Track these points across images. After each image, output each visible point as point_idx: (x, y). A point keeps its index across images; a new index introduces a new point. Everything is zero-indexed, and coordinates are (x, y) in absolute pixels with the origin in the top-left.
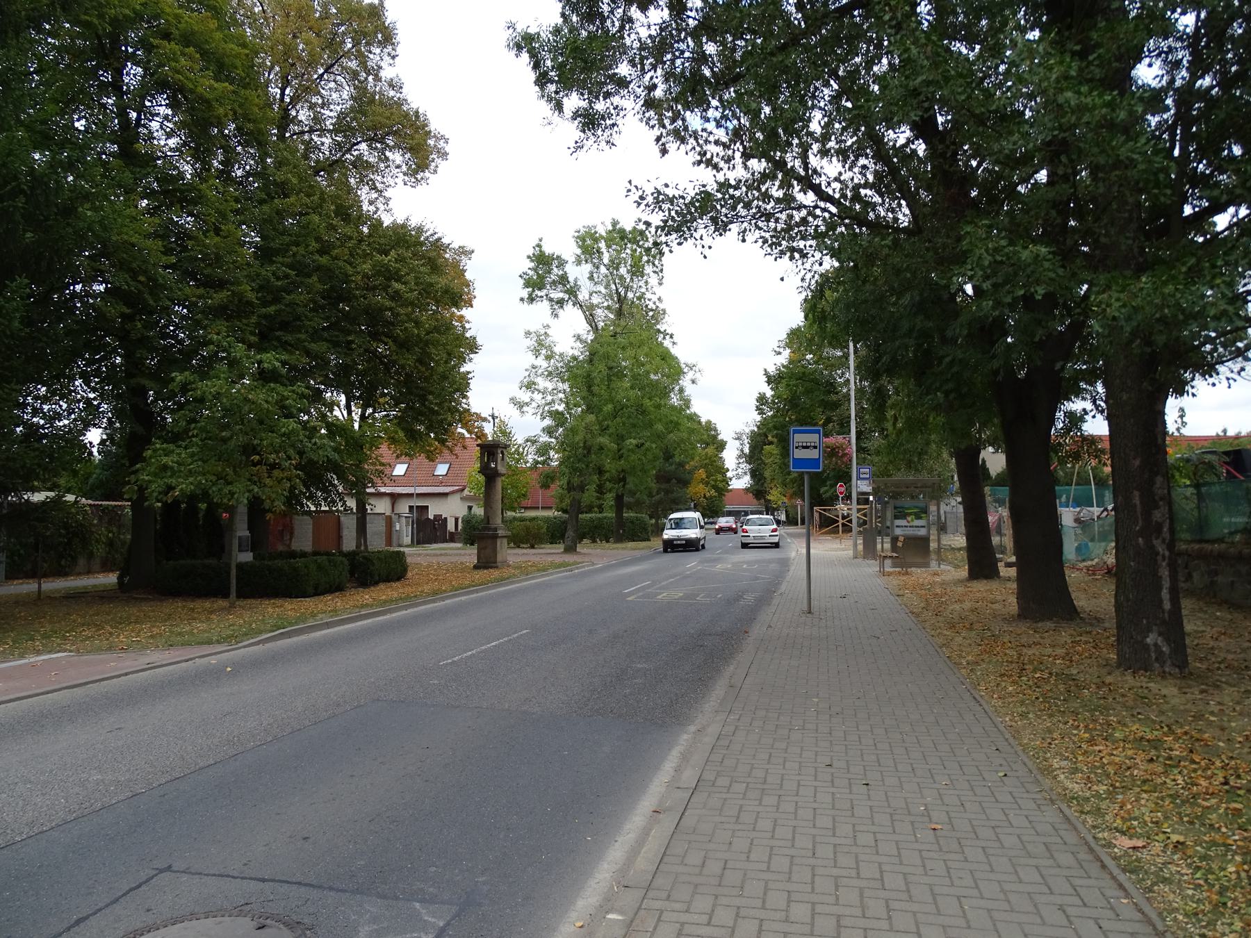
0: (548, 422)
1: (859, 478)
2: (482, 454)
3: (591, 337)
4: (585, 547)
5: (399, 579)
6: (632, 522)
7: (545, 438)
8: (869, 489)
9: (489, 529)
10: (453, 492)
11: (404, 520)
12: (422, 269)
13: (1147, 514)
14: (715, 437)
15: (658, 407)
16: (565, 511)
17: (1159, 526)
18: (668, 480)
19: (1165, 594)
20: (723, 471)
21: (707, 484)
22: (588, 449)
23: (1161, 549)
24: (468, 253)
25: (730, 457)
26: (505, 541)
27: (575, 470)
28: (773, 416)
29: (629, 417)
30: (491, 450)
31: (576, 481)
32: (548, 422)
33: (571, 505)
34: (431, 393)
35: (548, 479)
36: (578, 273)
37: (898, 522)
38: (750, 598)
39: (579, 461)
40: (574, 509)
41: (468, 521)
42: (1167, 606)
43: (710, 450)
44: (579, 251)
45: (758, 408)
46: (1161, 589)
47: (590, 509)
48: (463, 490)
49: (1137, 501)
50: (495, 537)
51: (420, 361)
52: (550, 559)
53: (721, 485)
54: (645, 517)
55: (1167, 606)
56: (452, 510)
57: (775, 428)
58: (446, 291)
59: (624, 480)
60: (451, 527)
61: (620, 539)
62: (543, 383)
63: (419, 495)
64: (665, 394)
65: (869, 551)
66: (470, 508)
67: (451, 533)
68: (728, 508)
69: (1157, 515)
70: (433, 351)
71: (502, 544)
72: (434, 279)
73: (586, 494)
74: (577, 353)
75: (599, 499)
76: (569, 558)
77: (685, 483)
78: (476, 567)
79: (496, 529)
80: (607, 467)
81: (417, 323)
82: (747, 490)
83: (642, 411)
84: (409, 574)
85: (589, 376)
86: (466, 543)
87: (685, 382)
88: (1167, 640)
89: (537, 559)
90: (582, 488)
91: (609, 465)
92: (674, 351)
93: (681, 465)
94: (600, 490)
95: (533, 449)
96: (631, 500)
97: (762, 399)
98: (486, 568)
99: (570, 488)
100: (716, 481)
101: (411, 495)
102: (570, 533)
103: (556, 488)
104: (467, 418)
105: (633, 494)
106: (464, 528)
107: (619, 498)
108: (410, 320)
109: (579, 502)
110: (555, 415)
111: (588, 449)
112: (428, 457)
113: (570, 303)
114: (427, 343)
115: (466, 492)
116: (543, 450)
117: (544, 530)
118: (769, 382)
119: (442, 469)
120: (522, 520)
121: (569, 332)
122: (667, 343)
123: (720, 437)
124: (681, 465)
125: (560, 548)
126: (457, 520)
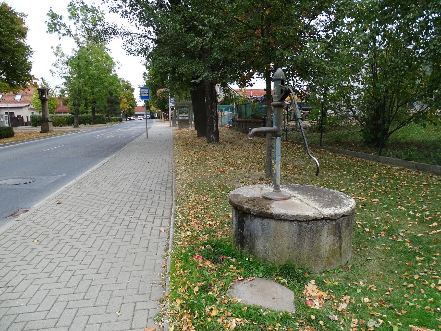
0: (64, 80)
1: (171, 102)
2: (39, 92)
3: (78, 49)
4: (82, 126)
5: (11, 137)
6: (99, 117)
7: (64, 87)
8: (174, 105)
9: (45, 119)
10: (25, 107)
11: (4, 117)
12: (9, 23)
13: (211, 110)
14: (130, 87)
15: (106, 77)
16: (73, 114)
17: (214, 112)
18: (112, 103)
19: (215, 127)
20: (134, 99)
21: (128, 104)
22: (80, 91)
23: (214, 117)
24: (25, 16)
25: (137, 94)
26: (52, 123)
27: (76, 99)
28: (149, 80)
29: (95, 80)
30: (43, 91)
31: (76, 102)
32: (64, 80)
33: (75, 111)
34: (17, 69)
35: (65, 102)
36: (71, 24)
37: (180, 115)
38: (133, 137)
39: (77, 95)
40: (77, 112)
41: (33, 118)
42: (215, 129)
43: (129, 91)
44: (70, 15)
45: (143, 77)
46: (214, 126)
47: (83, 113)
48: (29, 106)
49: (209, 107)
50: (48, 122)
51: (12, 58)
52: (69, 130)
53: (133, 104)
54: (105, 116)
55: (215, 129)
56: (25, 114)
57: (149, 84)
58: (19, 32)
59: (95, 102)
60: (25, 120)
61: (95, 123)
62: (61, 66)
63: (10, 108)
64: (109, 71)
65: (174, 125)
66: (32, 113)
67: (25, 122)
68: (136, 113)
69: (213, 110)
70: (17, 54)
71: (51, 125)
72: (14, 26)
73: (81, 107)
74: (73, 55)
75: (86, 109)
76: (75, 129)
77: (119, 104)
78: (41, 132)
79: (47, 119)
80: (88, 98)
81: (10, 44)
82: (143, 106)
83: (99, 77)
84: (15, 135)
85: (78, 64)
86: (33, 126)
87: (116, 68)
88: (215, 137)
89: (64, 130)
90: (79, 105)
91: (90, 98)
92: (111, 55)
93: (117, 97)
94: (86, 106)
95: (58, 90)
96: (98, 109)
97: (145, 74)
98: (45, 132)
99: (74, 105)
100: (131, 103)
101: (6, 108)
102: (76, 121)
103: (68, 106)
104: (31, 78)
105: (98, 107)
106: (32, 120)
107: (93, 109)
108: (7, 42)
109: (78, 110)
110: (67, 78)
111: (80, 91)
112: (14, 93)
113: (68, 36)
114: (14, 51)
115: (31, 106)
116: (62, 91)
117: (65, 120)
118: (147, 68)
119: (18, 97)
120: (56, 117)
121: (70, 48)
122: (108, 52)
123: (132, 87)
124: (117, 97)
125: (73, 126)
126: (27, 117)
